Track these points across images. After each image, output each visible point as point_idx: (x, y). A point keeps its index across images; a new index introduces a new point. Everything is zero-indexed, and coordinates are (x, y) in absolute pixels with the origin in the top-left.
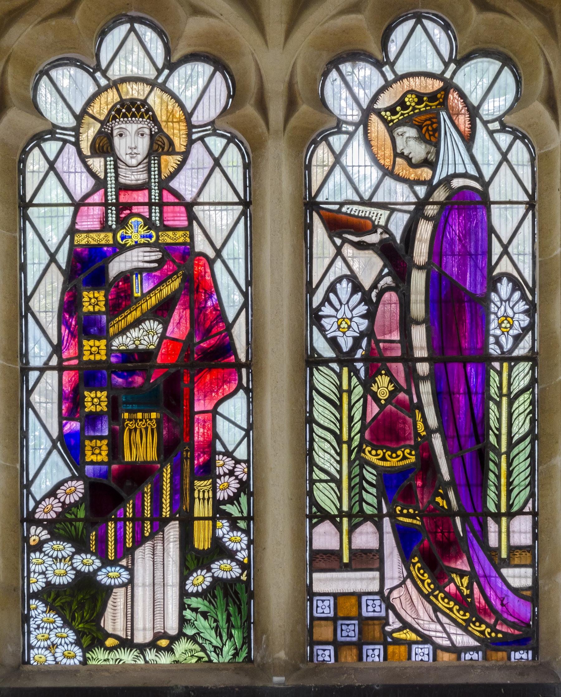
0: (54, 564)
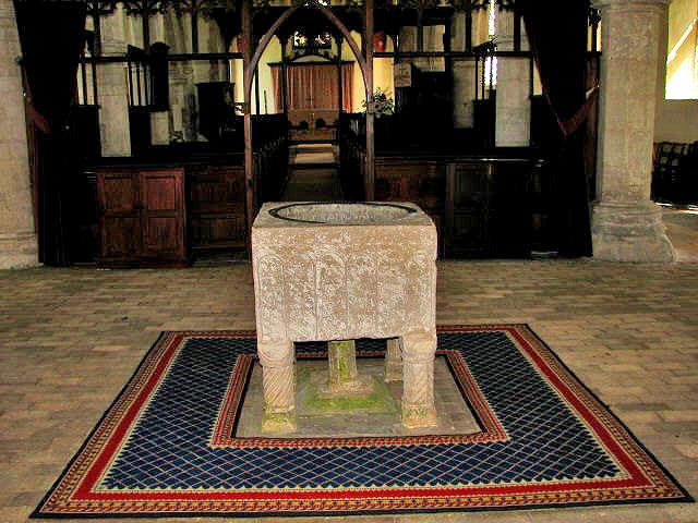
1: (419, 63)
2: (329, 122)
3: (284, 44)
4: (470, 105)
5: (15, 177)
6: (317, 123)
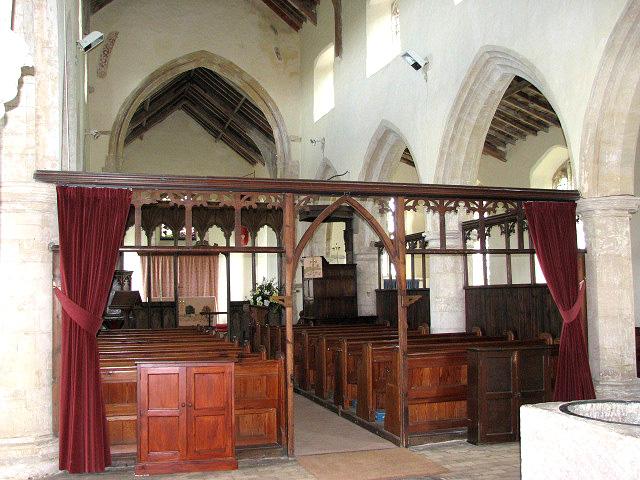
4: (374, 295)
5: (37, 373)
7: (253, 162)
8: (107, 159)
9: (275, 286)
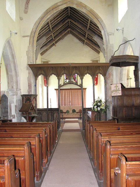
0: (65, 80)
1: (83, 55)
2: (77, 111)
3: (59, 79)
6: (73, 111)
7: (98, 52)
8: (29, 47)
9: (103, 100)
